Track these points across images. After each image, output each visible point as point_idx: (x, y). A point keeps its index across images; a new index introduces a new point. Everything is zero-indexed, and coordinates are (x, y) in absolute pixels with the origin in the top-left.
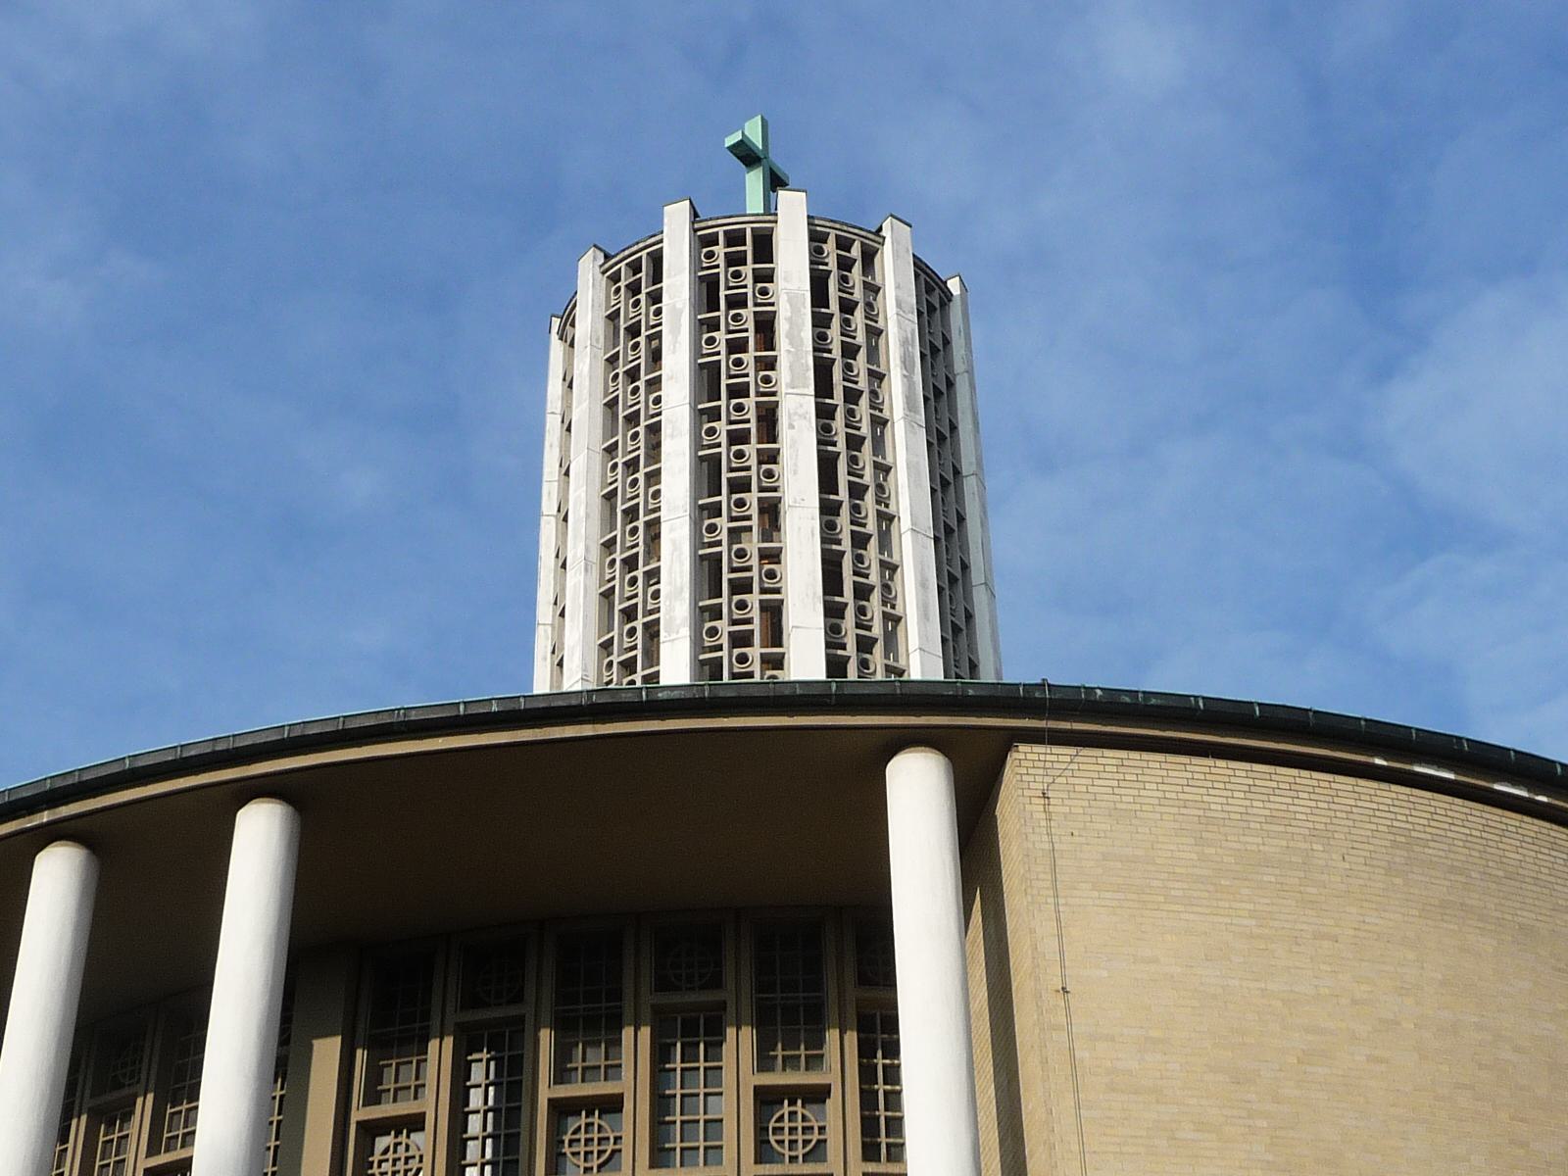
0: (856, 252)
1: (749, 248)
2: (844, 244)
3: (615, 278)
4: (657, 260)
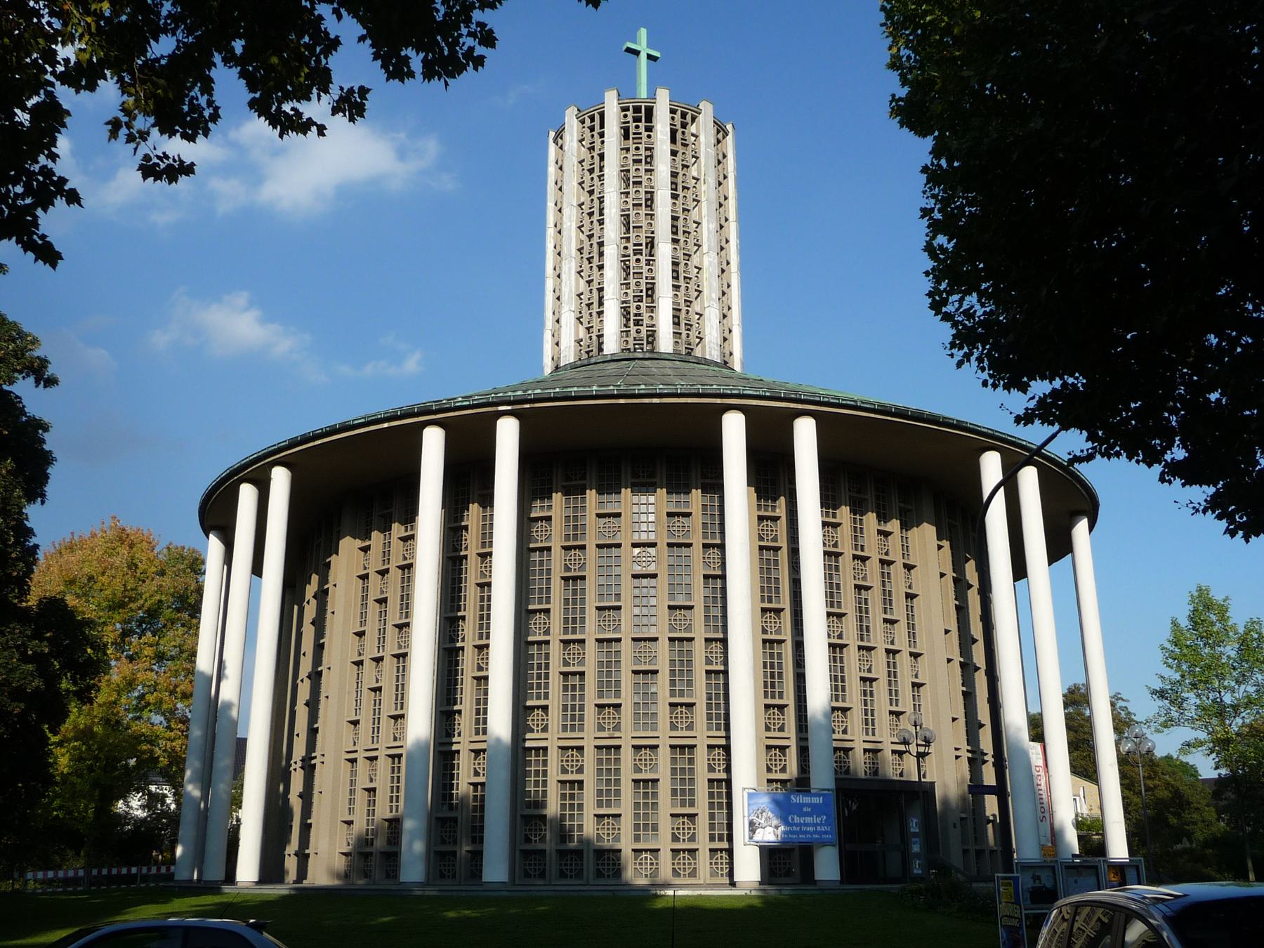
0: (689, 118)
1: (643, 114)
2: (684, 115)
3: (583, 122)
4: (602, 115)
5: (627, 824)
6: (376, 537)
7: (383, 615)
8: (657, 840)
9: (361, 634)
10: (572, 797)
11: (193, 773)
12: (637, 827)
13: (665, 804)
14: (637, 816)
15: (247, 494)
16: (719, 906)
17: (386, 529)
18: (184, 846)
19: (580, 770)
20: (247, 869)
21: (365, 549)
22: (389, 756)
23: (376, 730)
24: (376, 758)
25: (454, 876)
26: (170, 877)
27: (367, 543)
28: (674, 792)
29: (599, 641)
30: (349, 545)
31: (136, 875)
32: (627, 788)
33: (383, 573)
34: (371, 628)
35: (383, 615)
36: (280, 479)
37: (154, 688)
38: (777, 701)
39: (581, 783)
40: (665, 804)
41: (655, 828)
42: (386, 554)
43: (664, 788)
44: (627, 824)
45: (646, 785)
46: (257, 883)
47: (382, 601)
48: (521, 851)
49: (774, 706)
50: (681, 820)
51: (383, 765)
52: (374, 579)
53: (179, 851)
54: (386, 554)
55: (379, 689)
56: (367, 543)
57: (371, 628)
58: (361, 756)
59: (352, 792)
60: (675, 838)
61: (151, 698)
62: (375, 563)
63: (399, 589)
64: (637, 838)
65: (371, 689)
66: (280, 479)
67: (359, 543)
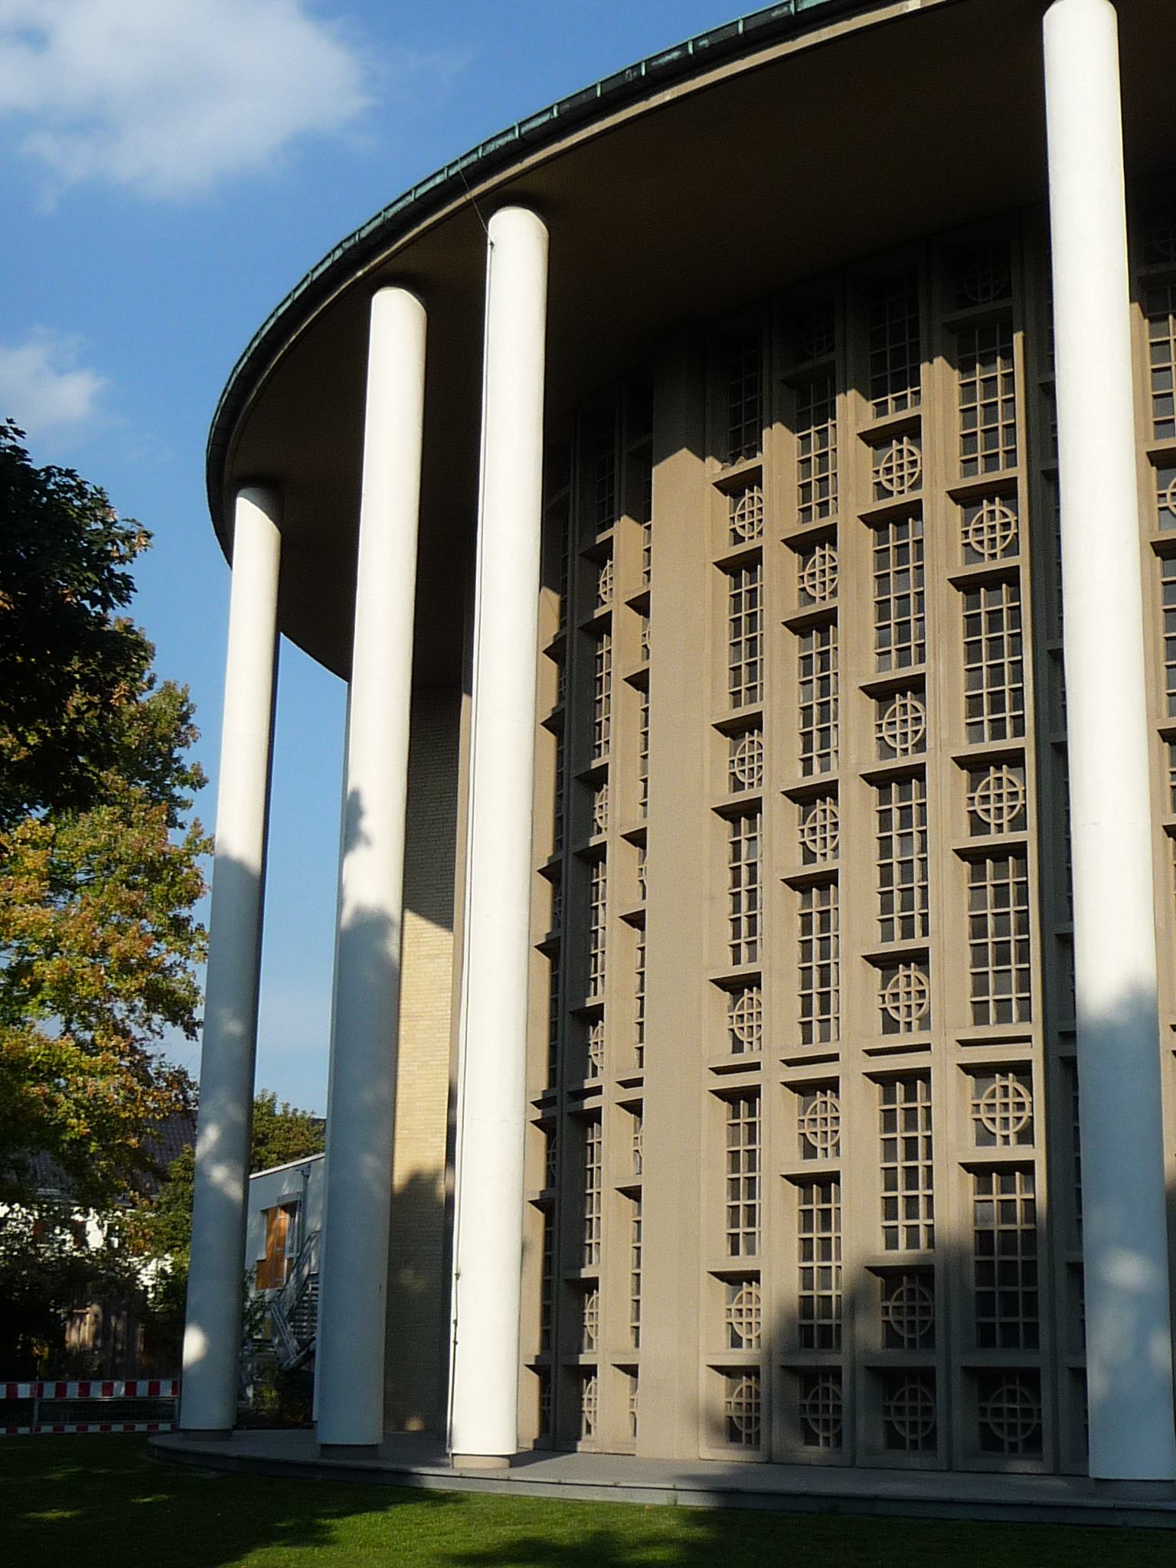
6: (779, 448)
7: (818, 671)
9: (737, 986)
11: (226, 1134)
15: (396, 323)
17: (811, 411)
18: (206, 1329)
20: (486, 1408)
21: (734, 488)
22: (874, 1077)
23: (818, 1002)
24: (831, 1085)
25: (930, 1442)
26: (156, 1410)
27: (744, 465)
30: (684, 480)
31: (29, 1402)
33: (803, 545)
34: (781, 699)
35: (818, 671)
36: (516, 250)
37: (52, 947)
42: (816, 489)
46: (515, 1460)
47: (816, 625)
48: (966, 1369)
51: (859, 1108)
52: (780, 822)
53: (193, 1344)
54: (816, 489)
55: (828, 880)
56: (744, 465)
57: (781, 699)
58: (771, 1080)
59: (743, 1185)
61: (47, 970)
62: (779, 511)
63: (871, 585)
65: (794, 883)
66: (516, 250)
67: (715, 469)
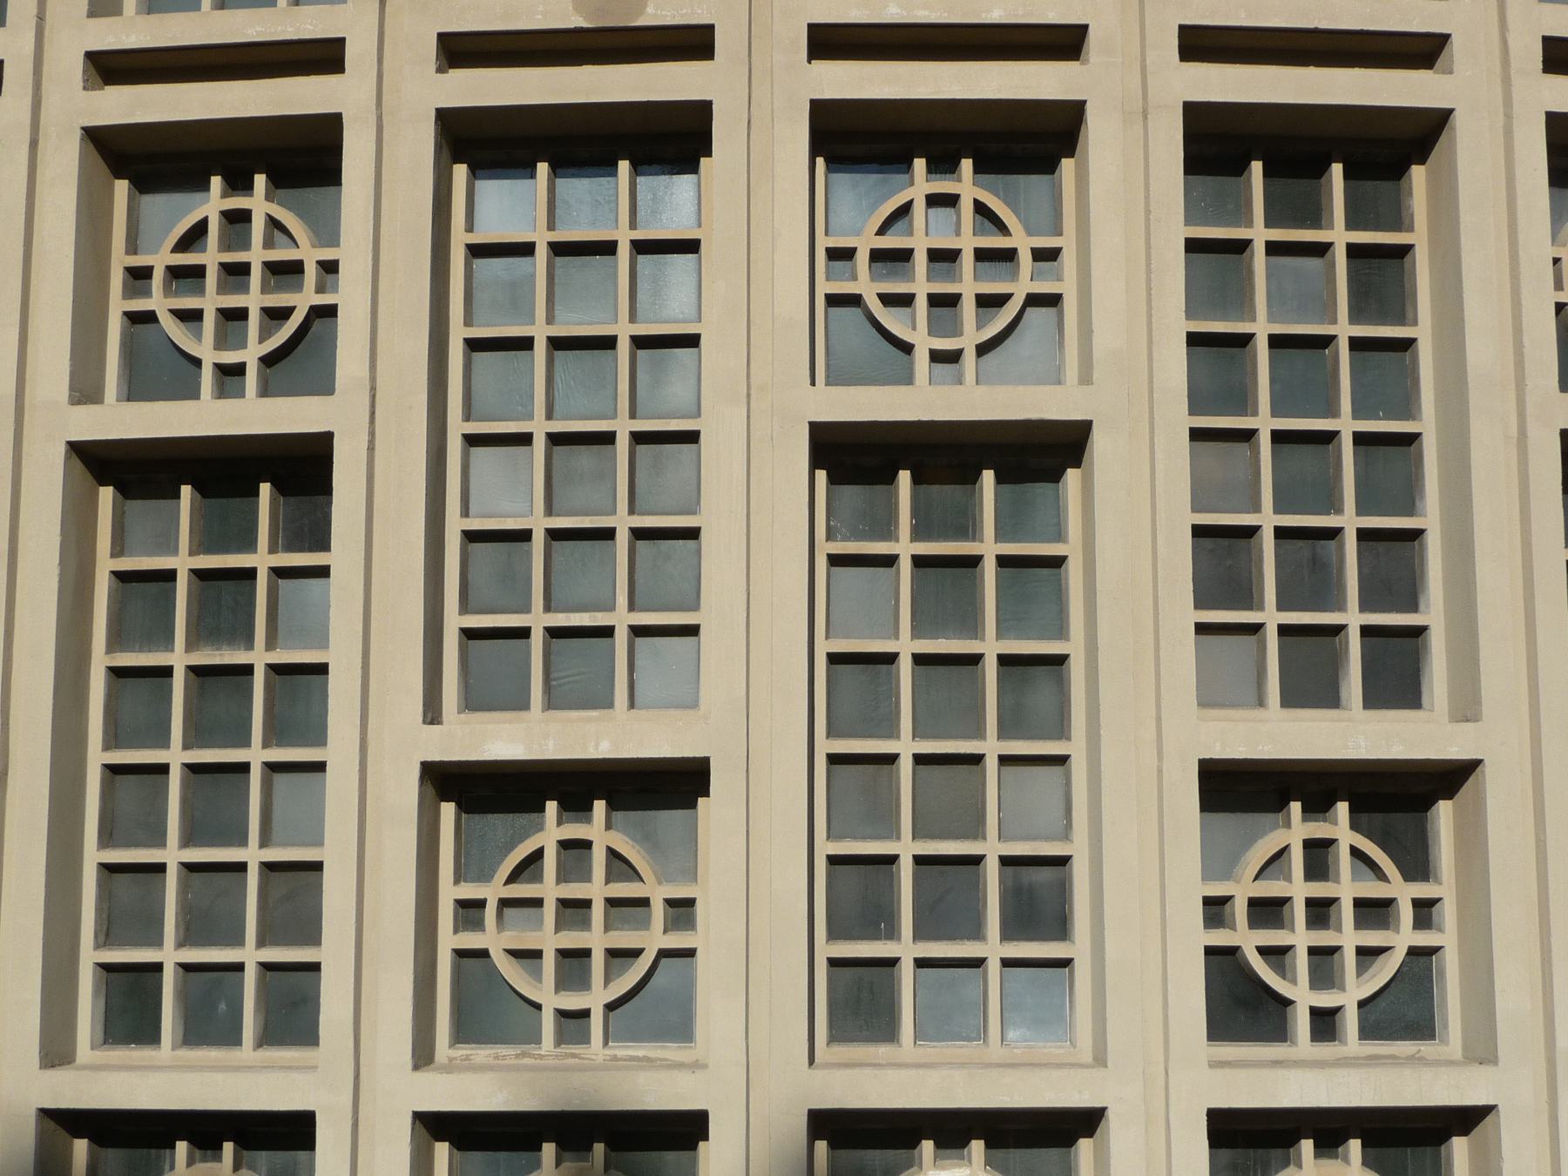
5: (754, 867)
8: (1055, 1020)
10: (224, 595)
12: (855, 890)
13: (1149, 699)
14: (855, 775)
16: (1077, 1165)
19: (301, 354)
28: (1221, 552)
29: (848, 455)
32: (757, 517)
38: (1354, 733)
39: (302, 468)
40: (1149, 699)
41: (1039, 897)
43: (1132, 520)
44: (754, 867)
45: (939, 480)
49: (1314, 785)
50: (1296, 828)
60: (1242, 1004)
64: (859, 1003)
